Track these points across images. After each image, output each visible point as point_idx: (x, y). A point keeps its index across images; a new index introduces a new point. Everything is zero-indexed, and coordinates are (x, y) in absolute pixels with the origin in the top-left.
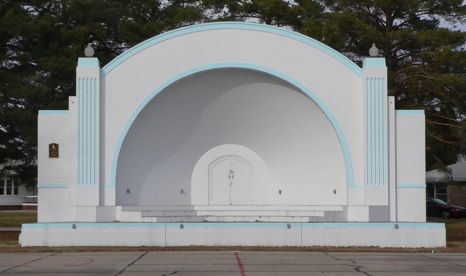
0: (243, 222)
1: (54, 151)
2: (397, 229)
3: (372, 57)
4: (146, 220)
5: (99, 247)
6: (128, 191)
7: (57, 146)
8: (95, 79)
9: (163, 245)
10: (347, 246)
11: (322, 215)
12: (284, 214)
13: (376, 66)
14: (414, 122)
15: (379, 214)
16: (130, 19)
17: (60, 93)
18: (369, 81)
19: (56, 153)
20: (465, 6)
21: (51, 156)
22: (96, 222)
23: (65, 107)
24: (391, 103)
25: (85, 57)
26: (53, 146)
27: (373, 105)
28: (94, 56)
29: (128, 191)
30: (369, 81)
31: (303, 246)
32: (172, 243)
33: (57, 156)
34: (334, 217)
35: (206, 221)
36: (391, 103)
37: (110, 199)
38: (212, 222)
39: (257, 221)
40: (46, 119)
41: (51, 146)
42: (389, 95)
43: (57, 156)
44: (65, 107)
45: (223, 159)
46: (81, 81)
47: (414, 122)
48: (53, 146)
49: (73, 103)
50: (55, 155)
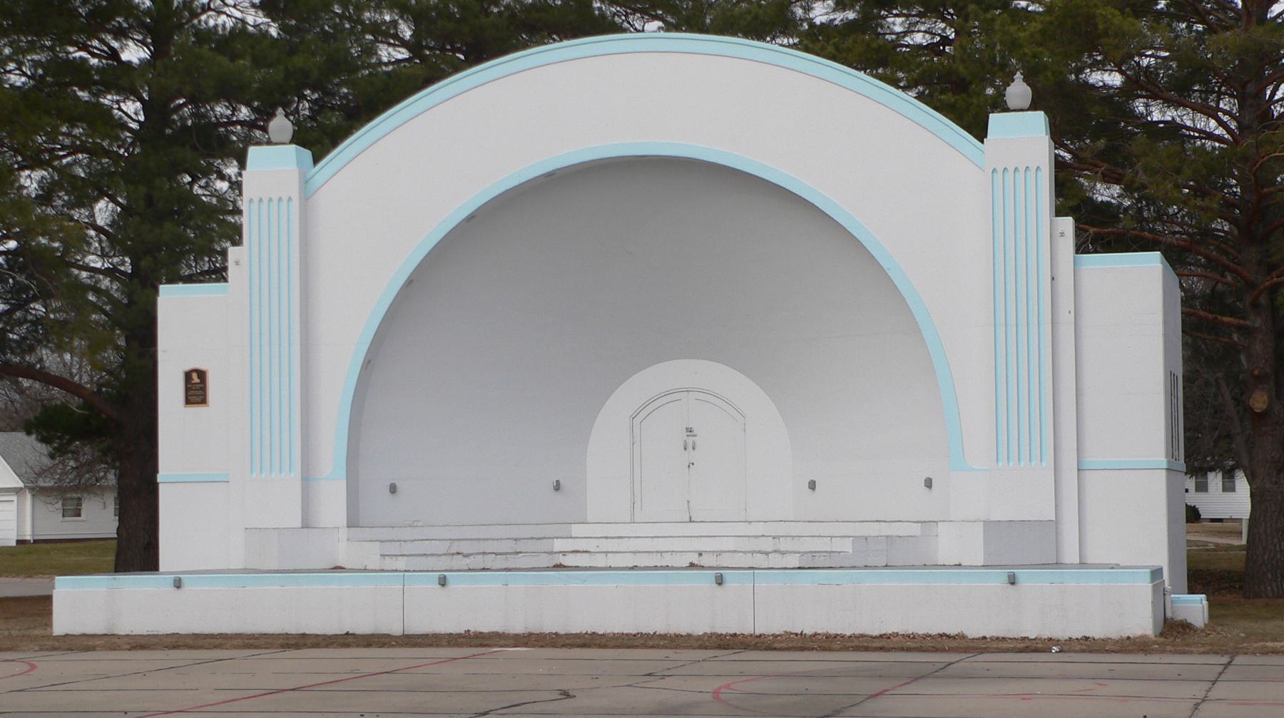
0: (656, 568)
1: (196, 388)
2: (174, 590)
3: (1014, 111)
4: (389, 563)
5: (196, 636)
6: (393, 489)
7: (202, 374)
8: (290, 199)
9: (396, 630)
10: (876, 633)
11: (847, 546)
12: (442, 548)
13: (1023, 135)
14: (1137, 289)
15: (1021, 549)
16: (708, 21)
17: (189, 238)
18: (998, 177)
19: (200, 392)
20: (268, 4)
21: (188, 402)
22: (984, 566)
23: (219, 274)
24: (1062, 234)
25: (1007, 110)
26: (195, 376)
27: (1010, 244)
28: (1034, 107)
29: (393, 489)
30: (998, 177)
31: (757, 633)
32: (420, 624)
33: (203, 401)
34: (888, 555)
35: (559, 567)
36: (1062, 234)
37: (332, 507)
38: (577, 568)
39: (692, 566)
40: (177, 305)
41: (188, 375)
42: (1059, 212)
43: (203, 401)
44: (219, 274)
45: (669, 398)
46: (255, 206)
47: (1137, 289)
48: (195, 376)
49: (237, 263)
50: (199, 399)
